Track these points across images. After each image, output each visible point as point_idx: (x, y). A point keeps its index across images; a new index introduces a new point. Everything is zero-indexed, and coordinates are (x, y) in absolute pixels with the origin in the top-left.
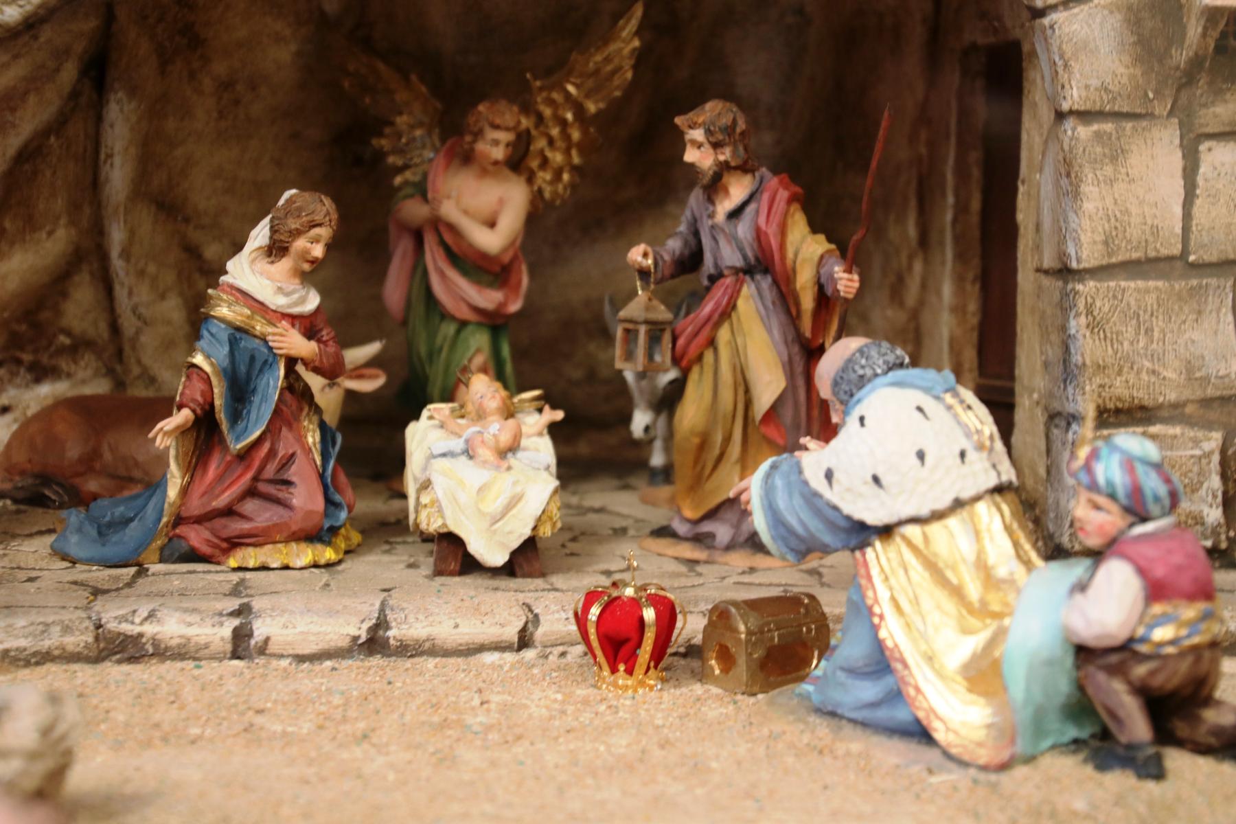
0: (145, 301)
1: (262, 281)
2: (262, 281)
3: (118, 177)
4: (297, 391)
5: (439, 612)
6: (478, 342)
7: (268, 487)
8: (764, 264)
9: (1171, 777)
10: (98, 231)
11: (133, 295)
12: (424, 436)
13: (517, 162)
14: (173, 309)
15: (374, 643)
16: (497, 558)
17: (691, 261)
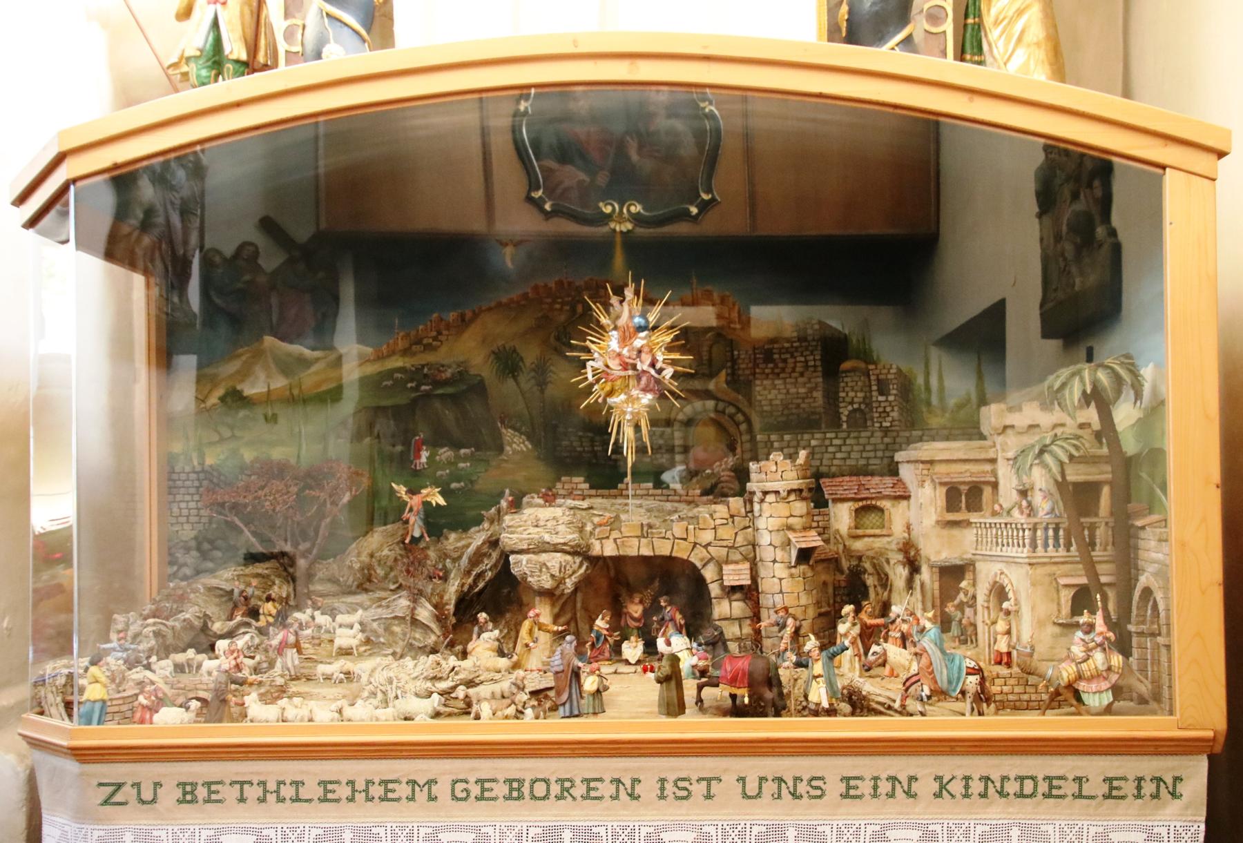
0: (583, 626)
1: (601, 624)
2: (601, 624)
3: (579, 605)
4: (606, 640)
5: (623, 668)
6: (635, 632)
7: (602, 653)
8: (672, 619)
9: (610, 712)
10: (575, 614)
11: (581, 625)
12: (625, 645)
13: (641, 602)
14: (587, 627)
15: (615, 672)
16: (633, 662)
17: (663, 619)
